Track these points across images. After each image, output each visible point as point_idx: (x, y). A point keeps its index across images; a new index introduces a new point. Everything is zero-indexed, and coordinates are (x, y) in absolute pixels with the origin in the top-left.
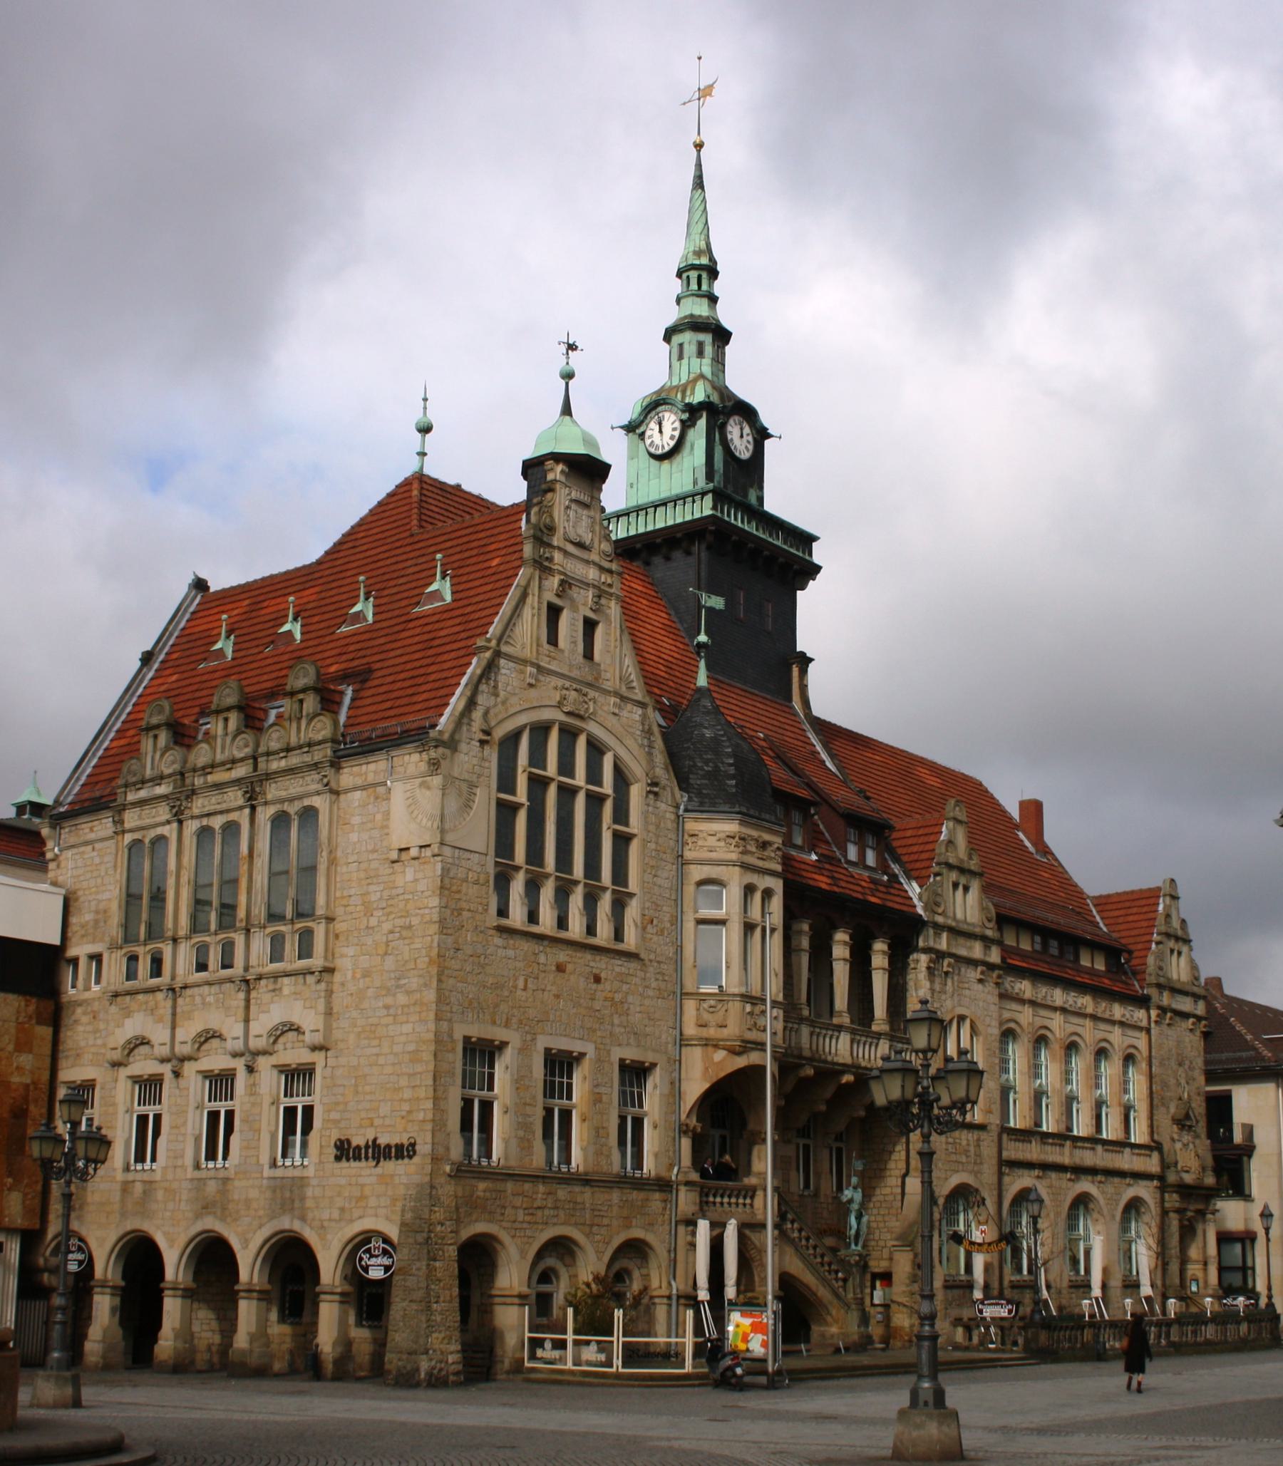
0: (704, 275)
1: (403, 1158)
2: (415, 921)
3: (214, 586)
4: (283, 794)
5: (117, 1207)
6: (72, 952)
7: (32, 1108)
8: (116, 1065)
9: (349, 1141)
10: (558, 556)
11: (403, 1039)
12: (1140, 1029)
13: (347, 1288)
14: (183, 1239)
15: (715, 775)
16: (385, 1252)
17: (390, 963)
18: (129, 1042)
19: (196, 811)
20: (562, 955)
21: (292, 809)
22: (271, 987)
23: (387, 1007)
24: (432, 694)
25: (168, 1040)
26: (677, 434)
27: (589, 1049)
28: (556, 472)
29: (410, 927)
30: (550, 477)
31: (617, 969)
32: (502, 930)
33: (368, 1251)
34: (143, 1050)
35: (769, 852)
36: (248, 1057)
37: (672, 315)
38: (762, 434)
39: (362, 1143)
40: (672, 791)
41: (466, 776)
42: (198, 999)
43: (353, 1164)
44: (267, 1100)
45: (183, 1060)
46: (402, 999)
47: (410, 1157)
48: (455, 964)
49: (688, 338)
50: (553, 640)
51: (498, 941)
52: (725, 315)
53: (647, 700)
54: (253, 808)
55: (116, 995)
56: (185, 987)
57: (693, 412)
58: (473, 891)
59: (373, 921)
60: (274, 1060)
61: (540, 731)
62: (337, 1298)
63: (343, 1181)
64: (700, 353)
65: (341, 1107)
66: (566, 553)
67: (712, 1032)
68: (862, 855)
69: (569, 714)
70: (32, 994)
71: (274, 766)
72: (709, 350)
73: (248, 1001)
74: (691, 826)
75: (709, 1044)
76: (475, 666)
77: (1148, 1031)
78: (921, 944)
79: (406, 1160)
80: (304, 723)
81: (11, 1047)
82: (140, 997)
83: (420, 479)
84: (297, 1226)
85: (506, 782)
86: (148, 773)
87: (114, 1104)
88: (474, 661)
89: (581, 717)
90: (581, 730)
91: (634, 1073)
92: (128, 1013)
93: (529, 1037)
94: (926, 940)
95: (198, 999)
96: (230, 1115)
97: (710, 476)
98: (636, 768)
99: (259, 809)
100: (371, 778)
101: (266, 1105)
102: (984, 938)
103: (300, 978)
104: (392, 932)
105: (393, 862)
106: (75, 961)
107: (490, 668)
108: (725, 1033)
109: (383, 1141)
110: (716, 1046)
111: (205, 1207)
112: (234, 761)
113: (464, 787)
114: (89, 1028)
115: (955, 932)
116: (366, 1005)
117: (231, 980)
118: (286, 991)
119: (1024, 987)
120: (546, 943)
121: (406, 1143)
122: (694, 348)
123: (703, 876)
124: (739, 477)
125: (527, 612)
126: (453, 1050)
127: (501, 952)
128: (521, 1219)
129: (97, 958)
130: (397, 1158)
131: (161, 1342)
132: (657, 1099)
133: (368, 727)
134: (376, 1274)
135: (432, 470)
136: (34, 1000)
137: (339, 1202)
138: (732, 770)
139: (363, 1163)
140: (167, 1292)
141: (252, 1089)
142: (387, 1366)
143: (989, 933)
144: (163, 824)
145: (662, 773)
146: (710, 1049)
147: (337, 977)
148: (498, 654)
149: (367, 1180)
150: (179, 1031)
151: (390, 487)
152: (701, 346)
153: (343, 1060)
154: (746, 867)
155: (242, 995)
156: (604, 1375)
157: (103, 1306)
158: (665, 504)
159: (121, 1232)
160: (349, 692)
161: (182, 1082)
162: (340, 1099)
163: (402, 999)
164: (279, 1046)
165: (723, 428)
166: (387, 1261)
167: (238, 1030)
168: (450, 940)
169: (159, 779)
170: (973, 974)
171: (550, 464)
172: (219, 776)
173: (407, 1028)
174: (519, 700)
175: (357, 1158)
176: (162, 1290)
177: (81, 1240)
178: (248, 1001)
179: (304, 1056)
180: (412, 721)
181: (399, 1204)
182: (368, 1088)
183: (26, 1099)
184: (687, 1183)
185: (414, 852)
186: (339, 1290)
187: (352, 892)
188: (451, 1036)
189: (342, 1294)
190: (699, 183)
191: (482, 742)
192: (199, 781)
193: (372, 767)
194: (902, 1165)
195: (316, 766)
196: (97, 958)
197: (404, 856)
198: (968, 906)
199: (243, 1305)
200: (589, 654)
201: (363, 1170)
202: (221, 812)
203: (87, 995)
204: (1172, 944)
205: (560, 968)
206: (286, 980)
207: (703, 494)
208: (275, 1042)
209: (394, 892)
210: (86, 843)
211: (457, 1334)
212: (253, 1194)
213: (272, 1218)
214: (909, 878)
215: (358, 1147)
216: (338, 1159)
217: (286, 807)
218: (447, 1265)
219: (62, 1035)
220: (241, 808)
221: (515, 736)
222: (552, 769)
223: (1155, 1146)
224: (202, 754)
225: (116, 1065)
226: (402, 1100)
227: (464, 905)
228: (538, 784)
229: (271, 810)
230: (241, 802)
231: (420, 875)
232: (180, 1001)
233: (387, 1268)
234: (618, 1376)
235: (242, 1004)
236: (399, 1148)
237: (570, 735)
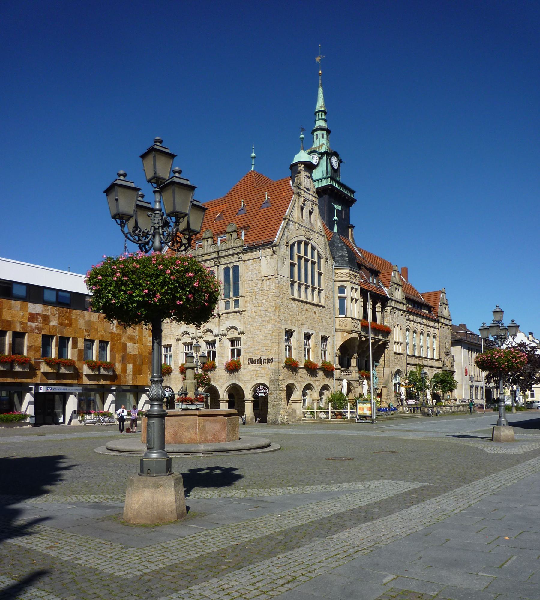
0: (323, 113)
2: (270, 296)
10: (302, 192)
11: (268, 329)
12: (437, 329)
15: (342, 257)
16: (264, 389)
20: (307, 306)
21: (231, 266)
23: (263, 321)
24: (271, 232)
26: (318, 161)
27: (314, 332)
28: (302, 167)
30: (299, 168)
32: (293, 299)
33: (259, 388)
39: (257, 359)
40: (330, 260)
41: (283, 255)
46: (267, 318)
48: (282, 308)
51: (292, 302)
53: (325, 235)
57: (322, 154)
58: (285, 288)
59: (257, 297)
61: (300, 243)
63: (251, 369)
64: (323, 137)
66: (305, 192)
67: (343, 328)
68: (373, 281)
69: (307, 238)
72: (325, 136)
74: (336, 271)
75: (342, 331)
76: (283, 223)
77: (438, 329)
78: (388, 305)
81: (148, 336)
84: (237, 382)
85: (292, 258)
88: (283, 222)
89: (310, 240)
90: (309, 243)
91: (324, 339)
94: (390, 303)
96: (214, 353)
97: (327, 173)
98: (323, 255)
100: (254, 257)
102: (403, 303)
108: (347, 328)
109: (263, 358)
114: (169, 330)
115: (396, 301)
116: (256, 320)
118: (231, 317)
119: (411, 317)
125: (295, 208)
126: (282, 333)
132: (330, 346)
133: (253, 242)
134: (262, 395)
137: (250, 375)
138: (347, 255)
143: (404, 302)
145: (329, 256)
152: (323, 135)
153: (249, 336)
154: (351, 282)
156: (326, 421)
160: (243, 232)
163: (267, 318)
165: (330, 159)
166: (265, 391)
168: (281, 301)
170: (400, 313)
171: (299, 165)
173: (269, 327)
174: (295, 233)
177: (170, 388)
180: (266, 240)
181: (269, 376)
184: (338, 369)
185: (269, 277)
191: (286, 246)
193: (255, 253)
195: (237, 254)
198: (398, 295)
200: (311, 222)
201: (257, 367)
204: (444, 306)
207: (327, 178)
215: (255, 360)
217: (228, 265)
221: (293, 244)
222: (303, 254)
223: (440, 360)
225: (179, 340)
226: (268, 347)
227: (284, 292)
228: (300, 258)
229: (224, 266)
233: (265, 393)
234: (330, 421)
237: (307, 244)
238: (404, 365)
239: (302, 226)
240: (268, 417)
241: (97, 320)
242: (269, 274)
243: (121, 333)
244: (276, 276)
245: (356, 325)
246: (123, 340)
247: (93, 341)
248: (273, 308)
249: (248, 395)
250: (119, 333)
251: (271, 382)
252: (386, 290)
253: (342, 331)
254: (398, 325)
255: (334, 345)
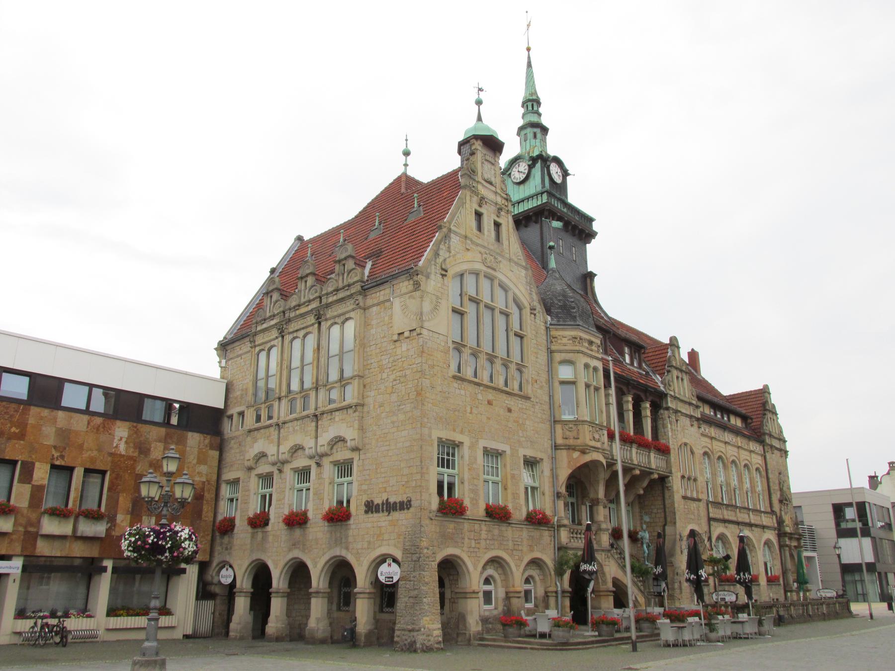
1: (404, 509)
2: (408, 372)
3: (306, 238)
4: (335, 313)
5: (248, 547)
6: (229, 413)
7: (206, 494)
8: (250, 469)
9: (372, 501)
13: (372, 590)
14: (282, 564)
17: (394, 397)
18: (256, 456)
19: (291, 330)
22: (329, 417)
23: (393, 422)
25: (275, 453)
29: (405, 376)
31: (520, 406)
34: (263, 459)
35: (594, 348)
36: (317, 458)
37: (521, 123)
38: (565, 173)
42: (291, 429)
43: (375, 515)
44: (327, 482)
45: (284, 463)
46: (401, 417)
47: (408, 509)
49: (529, 131)
50: (479, 228)
52: (544, 121)
54: (320, 323)
55: (250, 431)
56: (284, 423)
59: (385, 376)
60: (331, 459)
62: (367, 596)
63: (369, 525)
64: (535, 137)
65: (368, 482)
67: (571, 442)
70: (207, 434)
71: (330, 300)
73: (317, 427)
74: (554, 333)
75: (570, 448)
79: (406, 511)
80: (346, 275)
81: (195, 461)
82: (262, 431)
83: (405, 174)
86: (268, 315)
87: (249, 490)
89: (495, 270)
90: (496, 278)
92: (255, 440)
93: (474, 440)
95: (291, 429)
98: (525, 302)
99: (322, 323)
100: (382, 299)
101: (327, 484)
103: (345, 411)
104: (395, 380)
105: (395, 341)
106: (231, 417)
107: (446, 237)
109: (392, 500)
110: (574, 450)
111: (294, 545)
112: (310, 301)
113: (434, 298)
114: (237, 451)
117: (308, 416)
118: (337, 419)
120: (481, 388)
121: (405, 500)
122: (532, 135)
123: (562, 358)
124: (558, 190)
127: (458, 391)
128: (473, 545)
129: (242, 414)
130: (400, 510)
131: (269, 624)
135: (410, 173)
136: (209, 437)
139: (381, 514)
140: (273, 595)
141: (319, 475)
142: (396, 639)
144: (274, 339)
146: (571, 451)
147: (366, 409)
148: (450, 230)
149: (383, 524)
150: (281, 447)
151: (391, 181)
153: (369, 455)
155: (314, 424)
157: (242, 604)
158: (523, 201)
159: (250, 560)
161: (283, 475)
162: (367, 477)
163: (401, 417)
164: (334, 450)
165: (548, 168)
167: (312, 443)
169: (273, 317)
171: (473, 141)
172: (303, 310)
173: (404, 433)
175: (377, 511)
176: (270, 593)
178: (317, 427)
179: (348, 455)
182: (382, 470)
183: (203, 489)
185: (407, 334)
186: (368, 591)
187: (373, 361)
188: (430, 437)
189: (369, 593)
190: (529, 65)
192: (292, 315)
193: (382, 293)
194: (662, 520)
196: (242, 414)
197: (401, 337)
199: (314, 601)
201: (381, 519)
202: (303, 328)
203: (237, 433)
205: (490, 403)
206: (337, 413)
207: (542, 193)
208: (332, 449)
209: (396, 358)
210: (238, 356)
211: (438, 617)
212: (320, 535)
213: (330, 548)
214: (654, 373)
215: (378, 505)
216: (366, 512)
218: (431, 576)
219: (224, 456)
220: (313, 325)
224: (293, 302)
230: (313, 321)
231: (410, 347)
232: (282, 431)
235: (314, 428)
236: (402, 503)
238: (704, 521)
239: (477, 245)
240: (397, 633)
241: (84, 428)
242: (406, 329)
243: (136, 454)
244: (418, 331)
245: (597, 436)
246: (139, 468)
247: (71, 470)
248: (413, 396)
249: (362, 580)
250: (131, 454)
251: (405, 551)
252: (658, 379)
253: (570, 448)
254: (686, 444)
255: (554, 476)
